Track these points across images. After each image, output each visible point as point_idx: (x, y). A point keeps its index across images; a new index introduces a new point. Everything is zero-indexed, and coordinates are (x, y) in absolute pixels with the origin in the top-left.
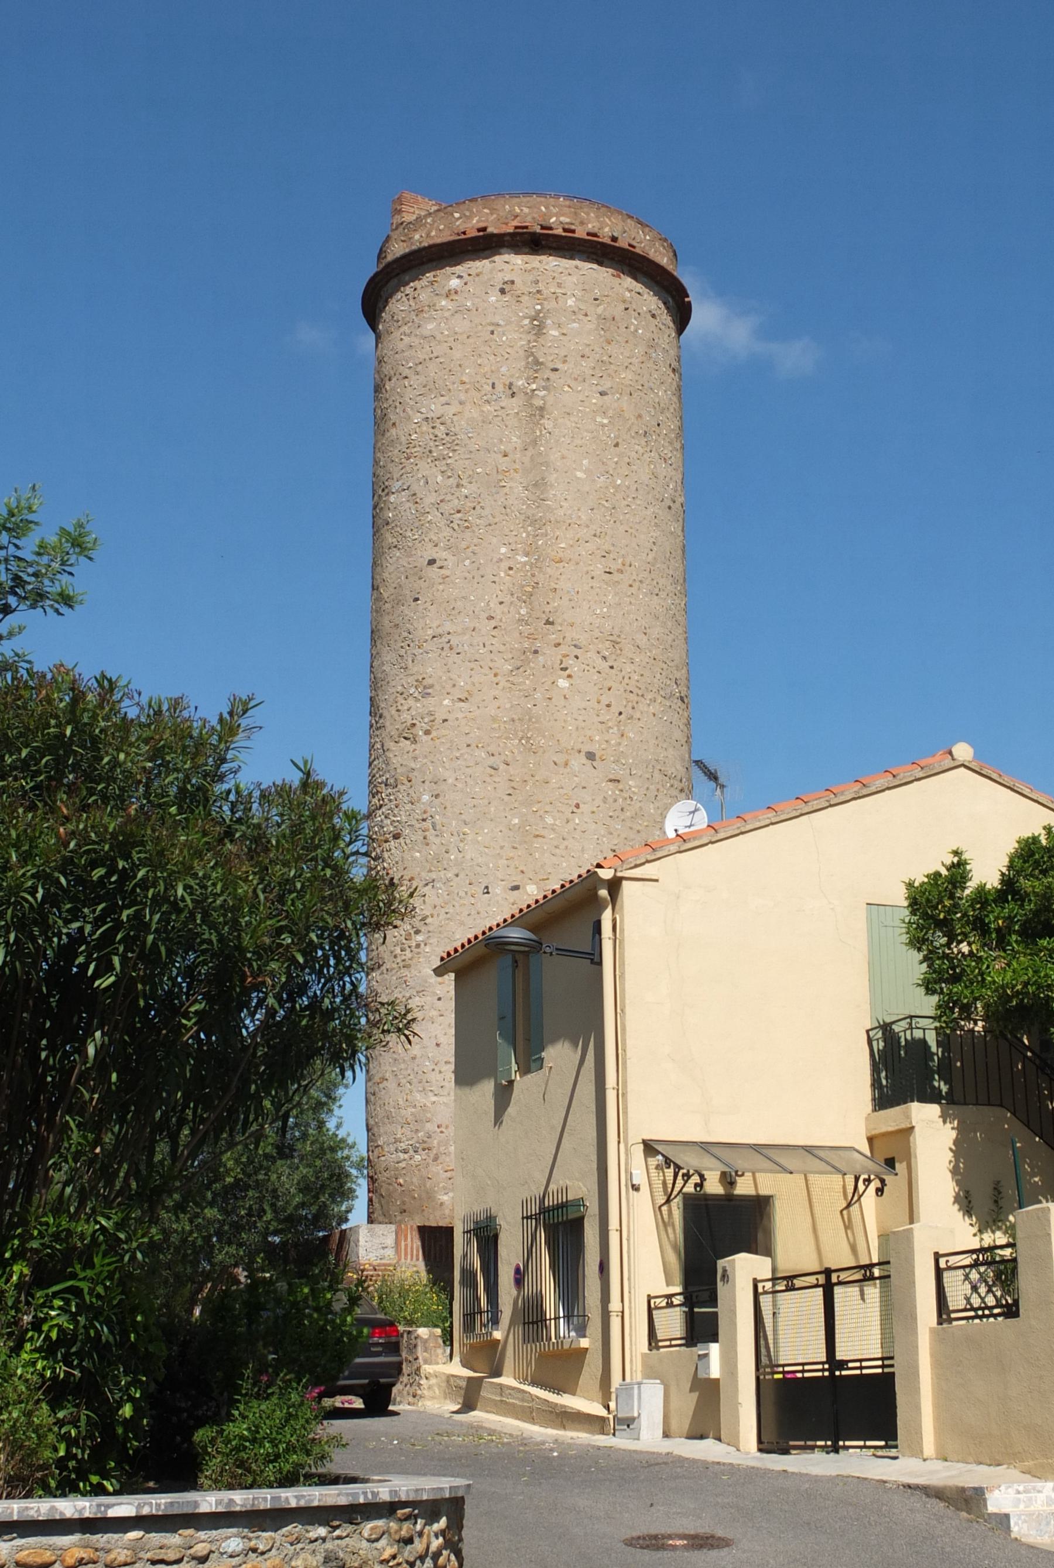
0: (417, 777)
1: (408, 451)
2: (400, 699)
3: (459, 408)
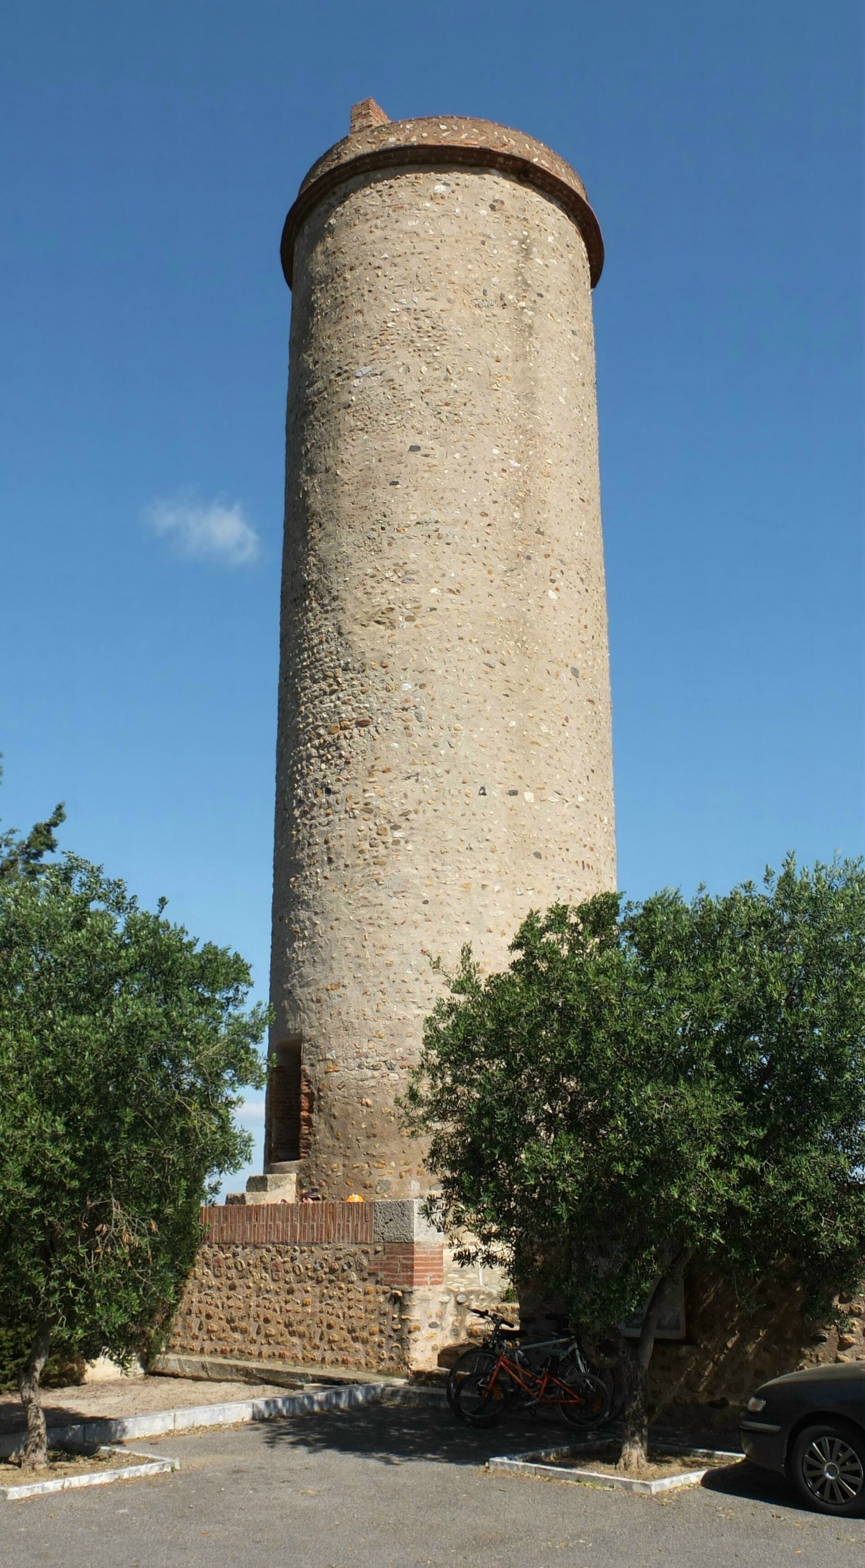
0: (395, 664)
1: (383, 338)
2: (370, 582)
3: (447, 306)
